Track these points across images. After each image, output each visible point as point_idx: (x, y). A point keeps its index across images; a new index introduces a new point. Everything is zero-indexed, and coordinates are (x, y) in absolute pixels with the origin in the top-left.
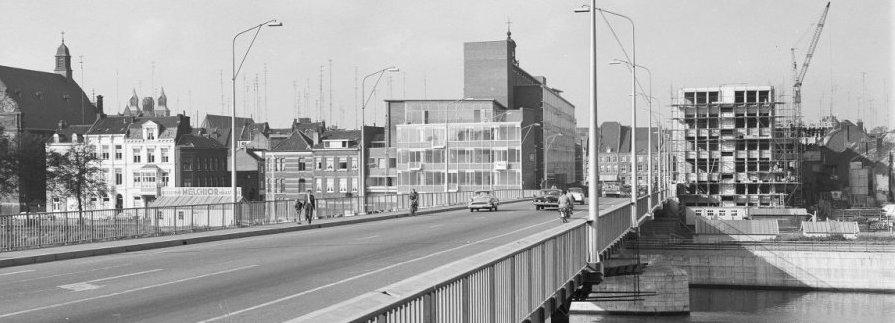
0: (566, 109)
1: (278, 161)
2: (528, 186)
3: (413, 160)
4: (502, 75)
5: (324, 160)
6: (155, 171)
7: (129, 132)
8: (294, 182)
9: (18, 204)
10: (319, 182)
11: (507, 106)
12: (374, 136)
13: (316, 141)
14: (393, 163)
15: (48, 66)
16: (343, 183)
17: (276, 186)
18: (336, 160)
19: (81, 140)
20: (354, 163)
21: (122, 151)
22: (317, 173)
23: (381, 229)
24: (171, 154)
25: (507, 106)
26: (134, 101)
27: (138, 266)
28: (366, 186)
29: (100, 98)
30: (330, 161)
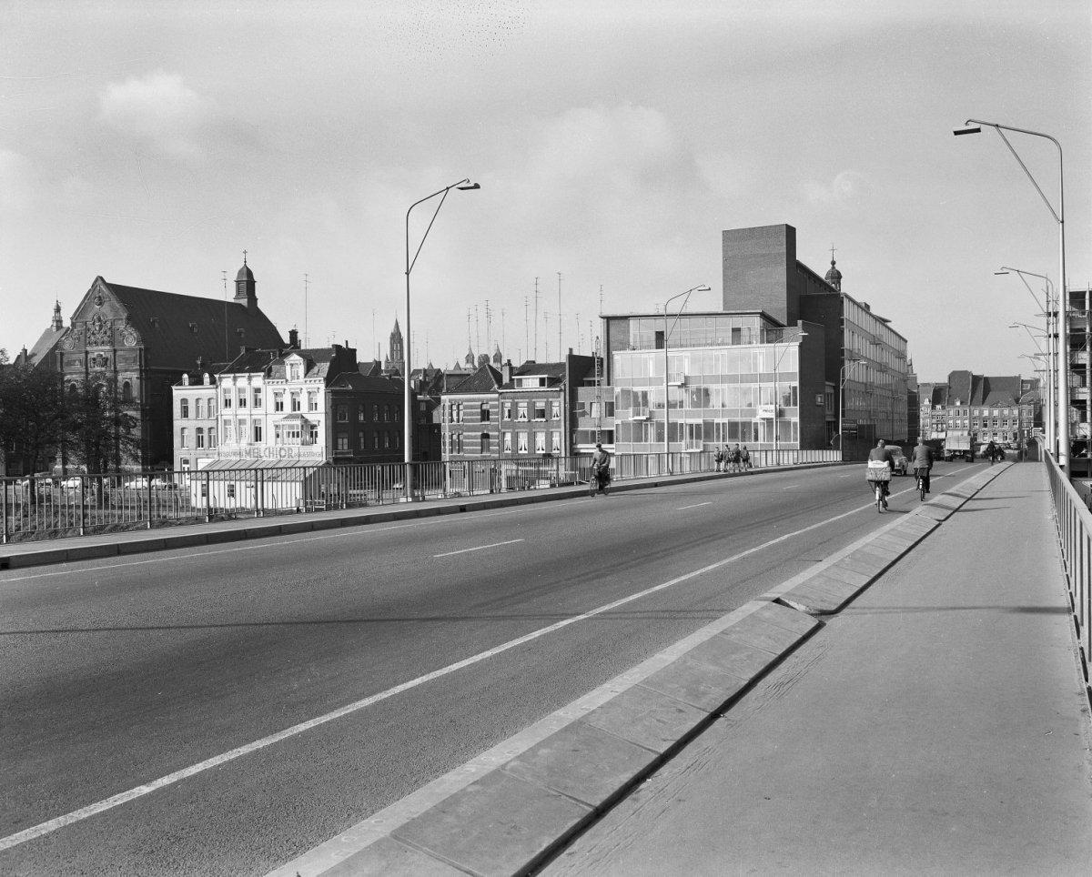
0: (892, 341)
1: (454, 407)
2: (807, 444)
3: (637, 404)
4: (780, 275)
5: (515, 405)
6: (298, 422)
7: (270, 370)
8: (475, 437)
9: (140, 467)
10: (508, 437)
11: (786, 324)
12: (582, 371)
13: (506, 380)
14: (610, 410)
15: (226, 292)
16: (541, 439)
17: (451, 444)
18: (531, 406)
19: (213, 382)
20: (555, 410)
21: (260, 396)
22: (505, 425)
23: (711, 492)
24: (321, 399)
25: (786, 324)
26: (470, 358)
27: (686, 494)
28: (572, 444)
29: (293, 334)
30: (523, 408)
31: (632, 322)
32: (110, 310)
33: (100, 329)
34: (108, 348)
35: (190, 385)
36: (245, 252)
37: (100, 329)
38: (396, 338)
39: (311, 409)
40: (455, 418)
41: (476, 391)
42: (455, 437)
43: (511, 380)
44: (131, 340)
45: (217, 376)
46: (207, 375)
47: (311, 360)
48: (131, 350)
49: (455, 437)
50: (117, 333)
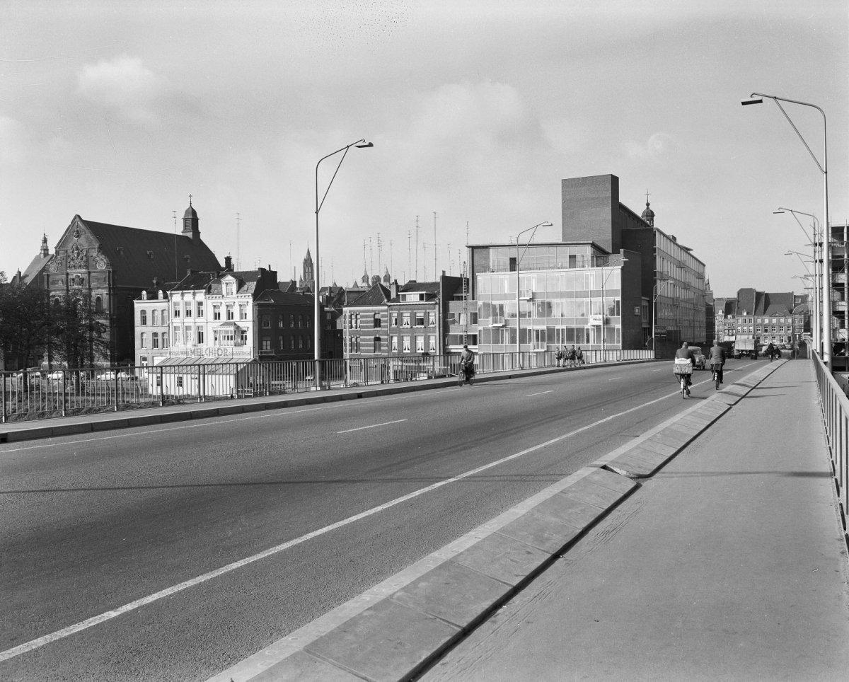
0: (694, 265)
1: (353, 317)
2: (628, 345)
3: (495, 314)
4: (606, 214)
5: (400, 315)
6: (232, 328)
7: (210, 288)
8: (369, 340)
9: (109, 363)
10: (395, 340)
11: (611, 252)
12: (453, 288)
13: (393, 295)
14: (474, 319)
15: (175, 227)
16: (420, 342)
17: (351, 345)
18: (413, 316)
19: (166, 297)
20: (432, 319)
21: (202, 308)
22: (393, 331)
23: (553, 383)
24: (249, 310)
25: (611, 252)
26: (365, 279)
27: (533, 384)
28: (445, 345)
29: (228, 260)
30: (406, 317)
31: (491, 251)
32: (86, 241)
33: (78, 256)
34: (84, 270)
35: (148, 299)
36: (191, 196)
37: (78, 256)
38: (308, 263)
39: (242, 318)
40: (354, 325)
41: (370, 304)
42: (354, 340)
43: (398, 295)
44: (102, 265)
45: (168, 292)
46: (161, 292)
47: (242, 280)
48: (102, 272)
49: (354, 340)
50: (91, 259)
